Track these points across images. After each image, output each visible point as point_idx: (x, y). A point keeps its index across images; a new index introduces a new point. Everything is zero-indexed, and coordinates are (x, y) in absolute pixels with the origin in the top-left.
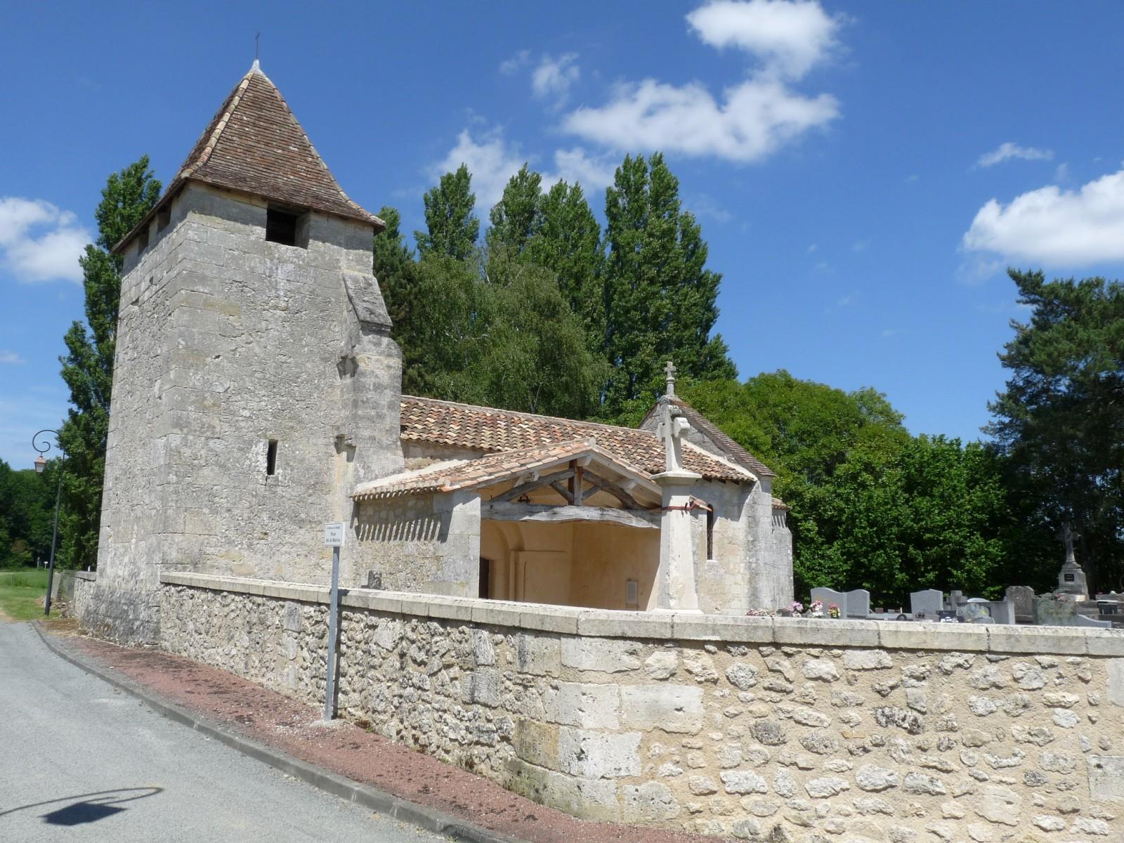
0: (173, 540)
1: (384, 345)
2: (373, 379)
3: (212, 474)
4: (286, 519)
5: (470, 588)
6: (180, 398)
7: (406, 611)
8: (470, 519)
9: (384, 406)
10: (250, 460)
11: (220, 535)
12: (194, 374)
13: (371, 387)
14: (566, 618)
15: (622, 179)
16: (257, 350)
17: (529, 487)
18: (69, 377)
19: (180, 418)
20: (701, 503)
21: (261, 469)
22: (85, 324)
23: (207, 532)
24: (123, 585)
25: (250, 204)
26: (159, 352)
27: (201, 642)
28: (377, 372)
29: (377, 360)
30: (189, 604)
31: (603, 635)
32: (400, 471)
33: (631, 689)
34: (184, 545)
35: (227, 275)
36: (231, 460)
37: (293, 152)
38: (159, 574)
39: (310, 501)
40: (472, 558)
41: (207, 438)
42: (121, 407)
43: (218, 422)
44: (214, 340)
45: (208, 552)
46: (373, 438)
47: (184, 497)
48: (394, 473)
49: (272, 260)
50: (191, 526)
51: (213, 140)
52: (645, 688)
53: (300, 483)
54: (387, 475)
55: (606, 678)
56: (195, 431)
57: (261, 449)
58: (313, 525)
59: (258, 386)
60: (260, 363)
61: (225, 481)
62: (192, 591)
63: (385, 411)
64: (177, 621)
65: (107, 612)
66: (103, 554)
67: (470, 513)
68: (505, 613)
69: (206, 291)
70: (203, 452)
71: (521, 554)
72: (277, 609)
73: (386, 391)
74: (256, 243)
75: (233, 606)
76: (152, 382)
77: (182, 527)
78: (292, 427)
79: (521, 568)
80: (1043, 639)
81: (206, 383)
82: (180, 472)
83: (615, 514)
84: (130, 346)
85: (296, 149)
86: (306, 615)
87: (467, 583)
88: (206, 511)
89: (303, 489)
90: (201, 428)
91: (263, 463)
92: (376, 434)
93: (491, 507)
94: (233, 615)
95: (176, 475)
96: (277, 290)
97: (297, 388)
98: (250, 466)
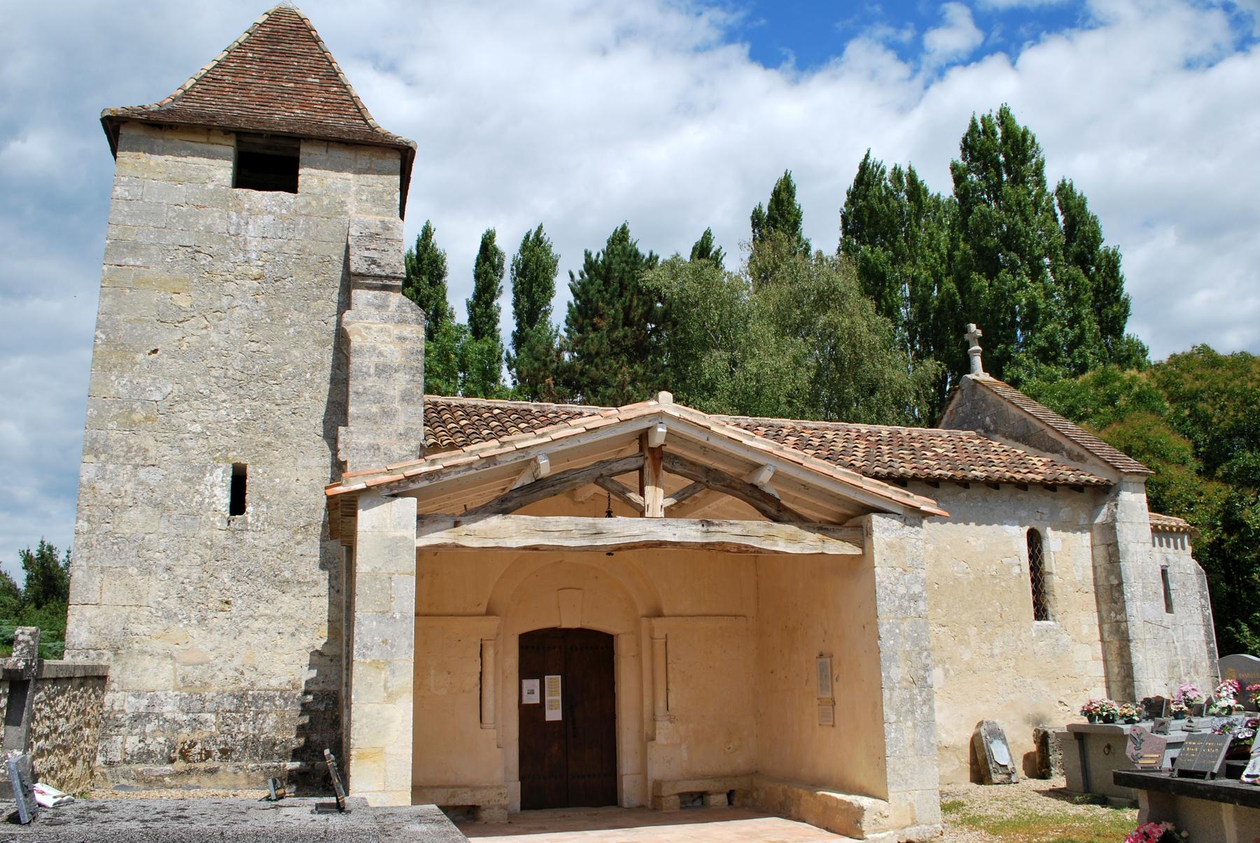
0: (82, 614)
1: (393, 307)
2: (375, 359)
3: (142, 518)
4: (260, 580)
5: (393, 672)
8: (393, 547)
9: (393, 397)
10: (201, 494)
11: (155, 605)
13: (372, 371)
16: (214, 337)
17: (542, 488)
19: (95, 440)
20: (924, 503)
21: (219, 507)
23: (133, 602)
25: (208, 142)
28: (382, 348)
34: (100, 622)
35: (170, 238)
37: (312, 83)
39: (298, 552)
40: (398, 616)
41: (136, 467)
44: (149, 328)
45: (135, 631)
47: (98, 552)
56: (118, 457)
58: (305, 588)
59: (215, 388)
60: (219, 355)
61: (163, 526)
63: (397, 405)
67: (393, 534)
69: (138, 263)
70: (128, 487)
73: (397, 375)
77: (97, 596)
78: (269, 444)
79: (659, 645)
80: (1081, 410)
83: (737, 530)
88: (133, 570)
89: (287, 533)
90: (127, 452)
91: (223, 498)
92: (382, 441)
95: (89, 521)
96: (246, 252)
97: (277, 387)
98: (201, 503)
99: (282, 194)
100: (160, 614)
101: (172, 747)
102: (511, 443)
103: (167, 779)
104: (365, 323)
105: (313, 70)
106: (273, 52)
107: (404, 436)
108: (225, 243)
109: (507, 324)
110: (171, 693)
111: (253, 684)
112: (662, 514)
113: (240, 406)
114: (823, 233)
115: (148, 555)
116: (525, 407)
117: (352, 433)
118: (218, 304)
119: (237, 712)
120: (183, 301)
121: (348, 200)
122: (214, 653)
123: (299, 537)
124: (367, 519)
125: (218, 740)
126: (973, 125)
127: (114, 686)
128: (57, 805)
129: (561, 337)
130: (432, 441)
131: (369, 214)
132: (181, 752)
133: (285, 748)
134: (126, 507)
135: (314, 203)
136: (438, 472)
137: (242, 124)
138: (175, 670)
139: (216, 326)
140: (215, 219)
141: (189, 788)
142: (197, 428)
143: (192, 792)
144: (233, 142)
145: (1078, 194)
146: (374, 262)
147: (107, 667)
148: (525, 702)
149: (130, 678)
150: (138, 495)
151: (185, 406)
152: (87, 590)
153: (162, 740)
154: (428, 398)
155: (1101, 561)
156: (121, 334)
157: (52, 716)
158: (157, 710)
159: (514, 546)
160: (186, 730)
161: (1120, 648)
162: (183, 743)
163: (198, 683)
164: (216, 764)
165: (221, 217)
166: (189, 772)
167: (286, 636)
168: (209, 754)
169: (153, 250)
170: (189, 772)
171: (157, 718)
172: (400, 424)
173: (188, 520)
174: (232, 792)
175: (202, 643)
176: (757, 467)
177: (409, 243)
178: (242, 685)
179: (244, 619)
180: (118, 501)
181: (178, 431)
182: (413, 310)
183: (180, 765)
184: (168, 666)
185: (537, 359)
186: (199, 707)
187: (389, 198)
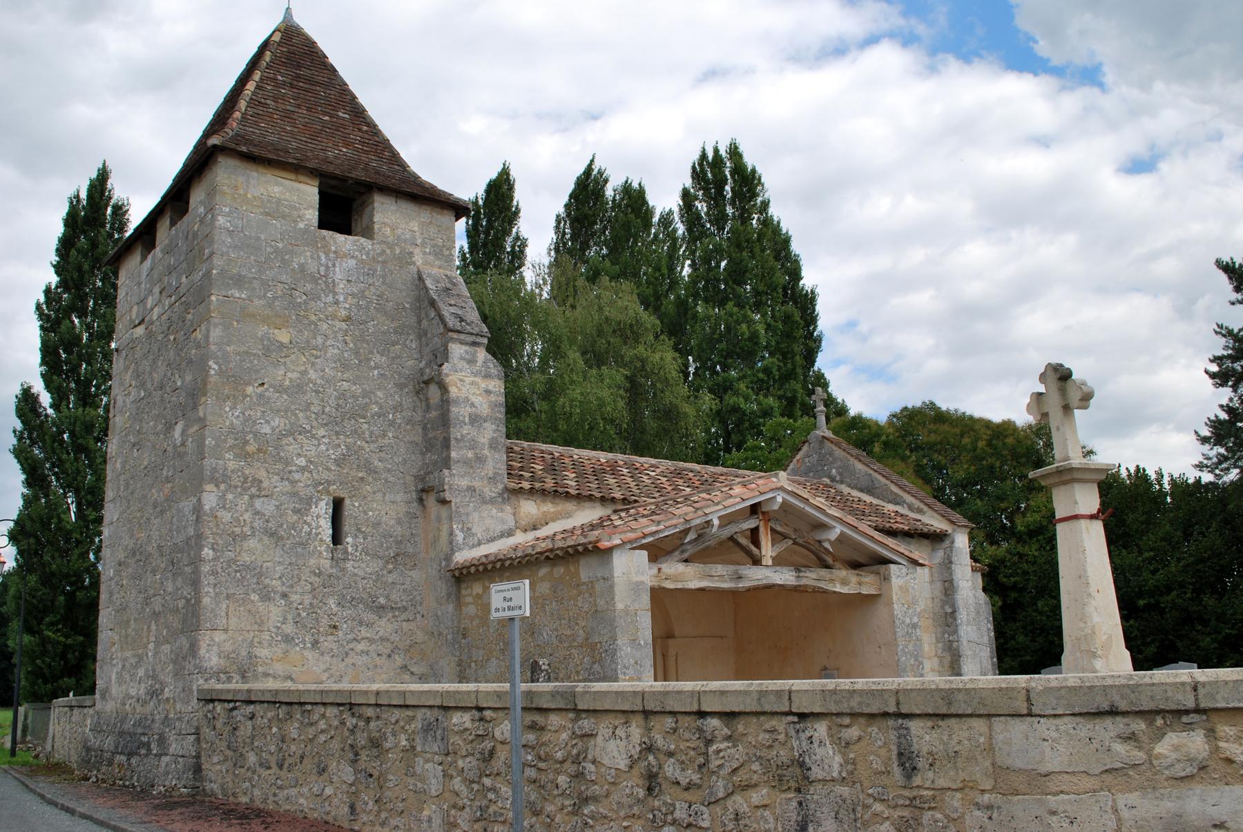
0: (212, 640)
1: (480, 363)
2: (469, 409)
3: (259, 546)
7: (650, 706)
8: (636, 588)
10: (309, 525)
11: (274, 630)
13: (467, 420)
14: (1001, 689)
15: (698, 175)
16: (312, 375)
18: (20, 453)
22: (39, 387)
24: (139, 709)
26: (179, 384)
27: (272, 779)
28: (473, 399)
29: (472, 383)
30: (246, 729)
31: (1077, 710)
32: (510, 533)
33: (1134, 798)
34: (228, 647)
35: (269, 274)
38: (195, 688)
39: (390, 580)
41: (252, 497)
42: (123, 467)
43: (264, 474)
46: (472, 489)
47: (223, 579)
48: (502, 536)
49: (327, 254)
51: (242, 104)
52: (1158, 795)
53: (375, 556)
54: (492, 540)
55: (1088, 783)
56: (236, 487)
57: (323, 509)
62: (251, 708)
63: (486, 452)
64: (228, 753)
65: (117, 747)
66: (105, 668)
68: (862, 692)
71: (671, 642)
72: (402, 724)
73: (485, 425)
74: (306, 231)
75: (322, 725)
76: (170, 427)
77: (224, 621)
78: (362, 478)
83: (814, 575)
84: (133, 383)
86: (456, 729)
88: (254, 597)
92: (477, 484)
94: (323, 738)
95: (213, 549)
96: (335, 294)
98: (310, 533)
107: (492, 480)
112: (770, 563)
114: (538, 228)
115: (267, 581)
120: (283, 336)
122: (326, 674)
123: (391, 566)
126: (704, 156)
131: (433, 266)
134: (244, 537)
135: (388, 251)
139: (313, 364)
140: (305, 257)
142: (302, 462)
145: (784, 231)
150: (256, 524)
155: (938, 593)
161: (952, 662)
167: (385, 657)
169: (256, 284)
176: (822, 526)
179: (348, 642)
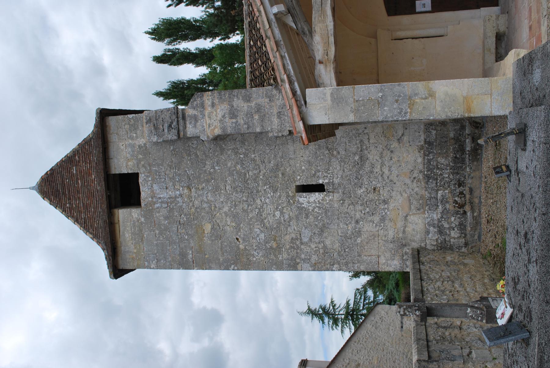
0: (384, 264)
1: (195, 112)
2: (227, 119)
3: (330, 238)
5: (416, 94)
6: (274, 266)
8: (337, 100)
9: (248, 106)
10: (314, 208)
12: (254, 257)
13: (234, 121)
16: (226, 209)
28: (220, 116)
29: (210, 117)
34: (388, 255)
36: (317, 223)
37: (76, 171)
39: (344, 153)
40: (380, 94)
41: (302, 243)
45: (392, 237)
47: (350, 258)
49: (155, 203)
50: (372, 251)
53: (329, 163)
56: (297, 253)
58: (364, 147)
60: (236, 205)
61: (333, 227)
63: (253, 104)
67: (329, 102)
69: (190, 252)
70: (313, 246)
73: (235, 106)
77: (374, 257)
78: (283, 174)
81: (259, 248)
82: (330, 263)
85: (74, 168)
87: (410, 98)
88: (359, 240)
89: (333, 160)
91: (316, 196)
92: (275, 111)
93: (321, 62)
95: (333, 265)
96: (176, 197)
97: (250, 173)
98: (319, 207)
99: (140, 180)
100: (382, 224)
101: (457, 213)
102: (265, 32)
103: (475, 214)
104: (206, 127)
105: (69, 171)
106: (64, 193)
107: (271, 99)
108: (173, 208)
109: (206, 44)
110: (426, 215)
111: (421, 172)
113: (263, 192)
115: (349, 232)
116: (247, 26)
117: (272, 129)
118: (207, 209)
119: (437, 179)
120: (208, 228)
121: (137, 144)
123: (335, 153)
124: (318, 117)
125: (453, 188)
127: (423, 245)
128: (513, 307)
129: (206, 8)
130: (272, 81)
132: (460, 208)
133: (458, 151)
134: (325, 247)
135: (142, 163)
136: (289, 77)
137: (105, 206)
138: (414, 214)
139: (220, 209)
140: (160, 215)
141: (480, 202)
142: (278, 213)
143: (483, 201)
144: (116, 211)
146: (170, 126)
147: (413, 249)
148: (429, 8)
149: (418, 237)
150: (317, 241)
151: (266, 221)
152: (371, 262)
153: (453, 219)
154: (248, 86)
156: (230, 257)
157: (442, 280)
158: (436, 222)
159: (332, 23)
160: (448, 206)
162: (454, 207)
163: (421, 202)
164: (467, 189)
165: (159, 212)
166: (471, 203)
167: (393, 155)
168: (461, 193)
169: (182, 245)
170: (471, 203)
171: (441, 222)
172: (264, 101)
173: (329, 214)
174: (483, 180)
175: (398, 201)
177: (169, 104)
178: (421, 178)
179: (384, 180)
180: (321, 251)
181: (280, 223)
182: (195, 100)
183: (467, 208)
184: (411, 218)
185: (221, 22)
186: (434, 200)
187: (132, 120)
